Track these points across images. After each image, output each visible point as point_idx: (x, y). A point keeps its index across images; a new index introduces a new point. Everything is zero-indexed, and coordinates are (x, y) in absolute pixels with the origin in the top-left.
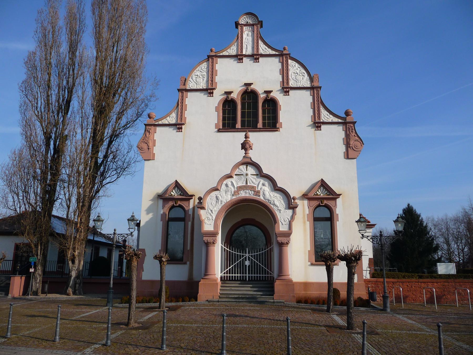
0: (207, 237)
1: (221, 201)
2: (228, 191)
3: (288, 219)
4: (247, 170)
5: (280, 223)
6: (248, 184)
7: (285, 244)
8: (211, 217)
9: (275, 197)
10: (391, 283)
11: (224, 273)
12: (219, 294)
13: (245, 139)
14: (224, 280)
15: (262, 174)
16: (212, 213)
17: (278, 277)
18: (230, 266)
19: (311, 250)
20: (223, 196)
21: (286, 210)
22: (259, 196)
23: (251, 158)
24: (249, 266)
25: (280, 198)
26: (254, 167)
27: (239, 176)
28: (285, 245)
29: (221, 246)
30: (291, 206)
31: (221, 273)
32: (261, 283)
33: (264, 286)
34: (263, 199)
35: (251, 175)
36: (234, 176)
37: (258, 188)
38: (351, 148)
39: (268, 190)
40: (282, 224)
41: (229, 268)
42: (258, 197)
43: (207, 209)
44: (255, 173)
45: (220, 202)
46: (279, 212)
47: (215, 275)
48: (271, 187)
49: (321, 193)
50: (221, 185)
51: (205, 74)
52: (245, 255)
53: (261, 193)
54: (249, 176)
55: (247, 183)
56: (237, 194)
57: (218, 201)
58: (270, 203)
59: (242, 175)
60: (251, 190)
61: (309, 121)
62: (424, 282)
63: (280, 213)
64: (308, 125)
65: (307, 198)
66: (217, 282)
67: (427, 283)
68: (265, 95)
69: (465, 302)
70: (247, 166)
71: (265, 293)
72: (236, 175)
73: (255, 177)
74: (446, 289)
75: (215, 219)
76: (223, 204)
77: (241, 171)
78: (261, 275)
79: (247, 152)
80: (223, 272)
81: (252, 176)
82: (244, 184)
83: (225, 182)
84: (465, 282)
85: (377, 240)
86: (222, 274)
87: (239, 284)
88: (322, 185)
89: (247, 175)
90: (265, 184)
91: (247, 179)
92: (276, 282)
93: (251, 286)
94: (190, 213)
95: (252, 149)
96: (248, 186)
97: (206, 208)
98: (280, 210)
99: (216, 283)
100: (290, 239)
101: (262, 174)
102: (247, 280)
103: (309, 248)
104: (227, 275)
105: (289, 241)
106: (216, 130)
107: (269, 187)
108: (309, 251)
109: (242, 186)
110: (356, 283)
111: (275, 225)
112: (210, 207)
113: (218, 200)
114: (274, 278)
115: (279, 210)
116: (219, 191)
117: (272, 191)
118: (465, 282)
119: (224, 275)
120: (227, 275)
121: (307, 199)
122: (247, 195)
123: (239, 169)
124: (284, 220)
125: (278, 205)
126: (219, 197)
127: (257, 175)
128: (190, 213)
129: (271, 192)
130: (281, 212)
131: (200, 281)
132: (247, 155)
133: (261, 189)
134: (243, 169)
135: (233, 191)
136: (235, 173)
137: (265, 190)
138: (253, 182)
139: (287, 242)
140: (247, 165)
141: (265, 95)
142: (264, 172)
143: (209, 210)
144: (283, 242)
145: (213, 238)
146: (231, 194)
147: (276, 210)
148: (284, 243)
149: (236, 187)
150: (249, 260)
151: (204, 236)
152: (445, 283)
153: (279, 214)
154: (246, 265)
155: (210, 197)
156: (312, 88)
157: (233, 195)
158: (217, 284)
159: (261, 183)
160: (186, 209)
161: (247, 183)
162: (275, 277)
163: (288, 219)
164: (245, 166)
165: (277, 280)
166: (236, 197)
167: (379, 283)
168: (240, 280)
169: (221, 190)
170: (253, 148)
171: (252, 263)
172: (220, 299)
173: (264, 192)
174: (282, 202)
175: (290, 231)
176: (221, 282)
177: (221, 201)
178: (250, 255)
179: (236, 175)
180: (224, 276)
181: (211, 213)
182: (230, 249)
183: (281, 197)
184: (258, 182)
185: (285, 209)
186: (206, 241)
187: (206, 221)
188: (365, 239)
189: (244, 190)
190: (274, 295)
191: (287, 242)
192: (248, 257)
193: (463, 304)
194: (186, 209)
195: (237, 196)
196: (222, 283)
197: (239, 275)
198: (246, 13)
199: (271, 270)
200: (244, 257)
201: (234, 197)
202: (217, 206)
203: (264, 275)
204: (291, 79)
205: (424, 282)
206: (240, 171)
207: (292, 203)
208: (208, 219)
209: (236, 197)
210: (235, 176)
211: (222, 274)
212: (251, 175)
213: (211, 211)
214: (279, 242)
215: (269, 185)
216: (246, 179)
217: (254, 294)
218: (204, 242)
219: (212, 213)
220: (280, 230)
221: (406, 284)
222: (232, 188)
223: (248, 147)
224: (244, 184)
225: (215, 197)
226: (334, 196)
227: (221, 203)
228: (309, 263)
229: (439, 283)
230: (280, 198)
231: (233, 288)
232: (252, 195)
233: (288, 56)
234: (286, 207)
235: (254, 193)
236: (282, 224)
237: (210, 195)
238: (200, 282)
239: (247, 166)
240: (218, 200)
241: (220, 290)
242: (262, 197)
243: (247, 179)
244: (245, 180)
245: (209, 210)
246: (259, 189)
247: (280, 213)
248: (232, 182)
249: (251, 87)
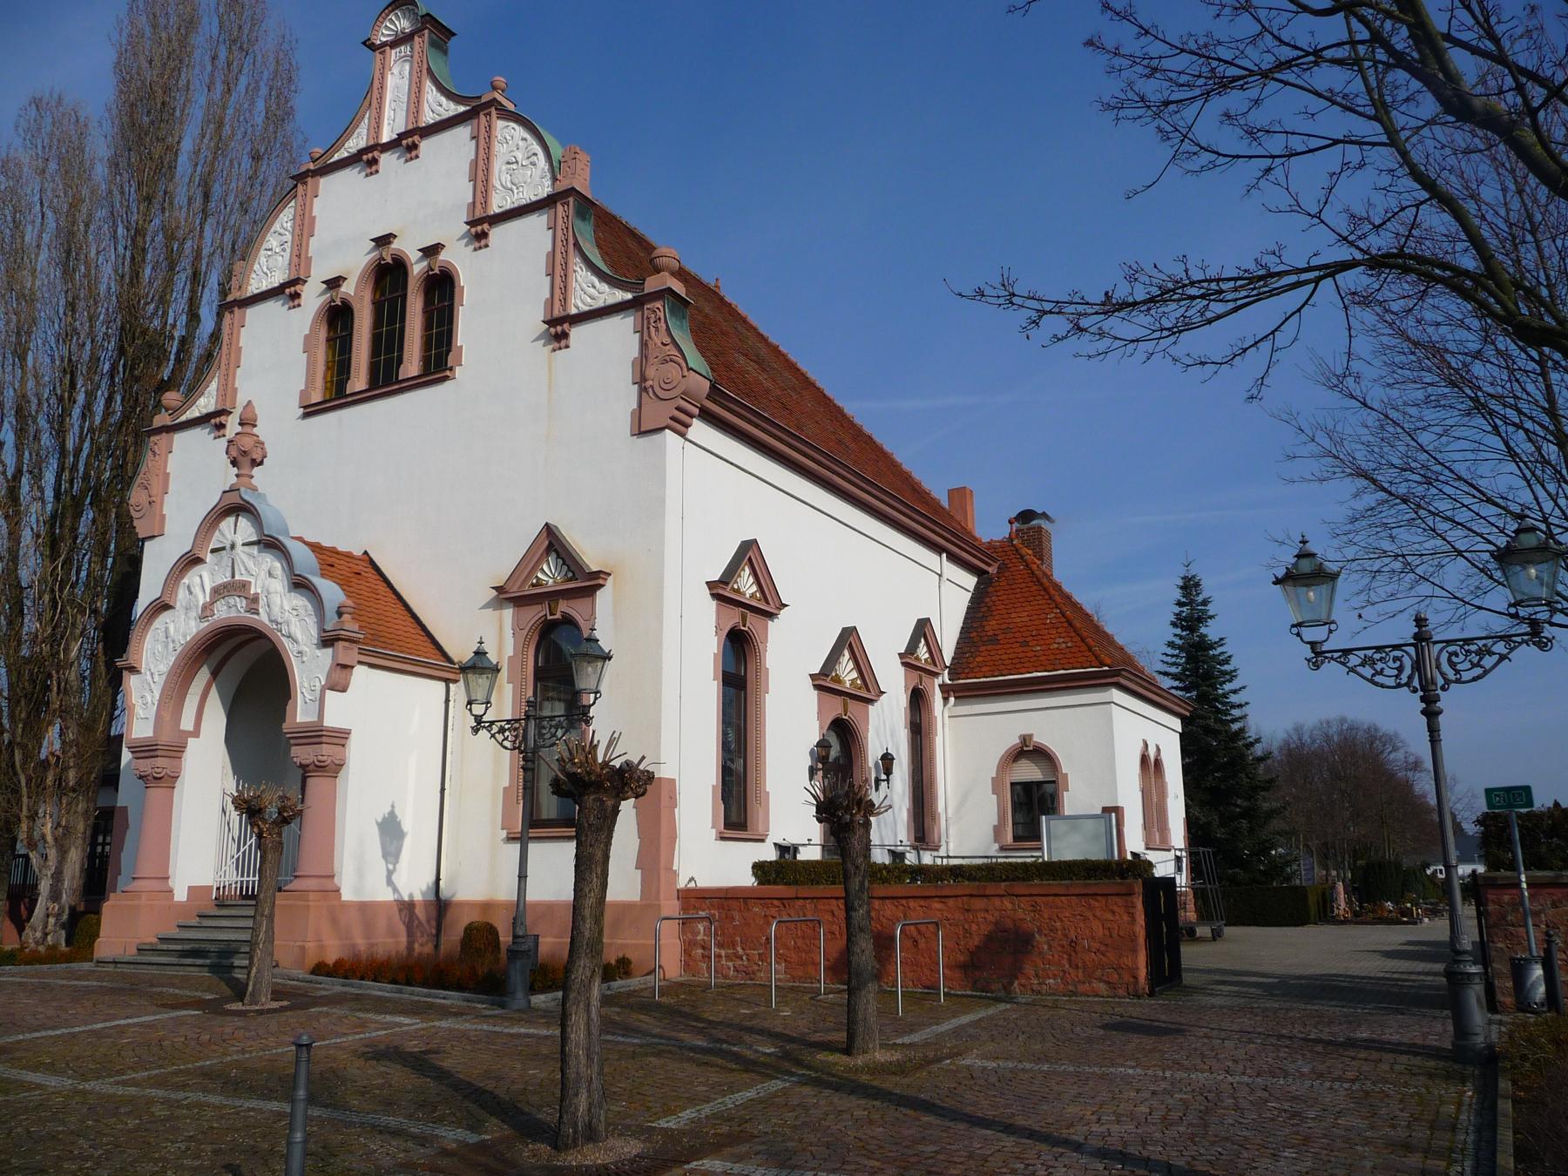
10: (776, 902)
18: (244, 845)
19: (510, 786)
23: (224, 492)
34: (267, 622)
35: (243, 545)
36: (209, 558)
38: (651, 394)
49: (549, 574)
51: (288, 237)
54: (239, 548)
61: (534, 318)
62: (893, 898)
64: (534, 337)
67: (904, 902)
68: (425, 263)
69: (1051, 981)
72: (213, 551)
73: (254, 550)
74: (974, 927)
81: (246, 549)
84: (1055, 895)
85: (516, 737)
88: (551, 548)
91: (233, 559)
103: (506, 782)
108: (505, 788)
110: (626, 907)
118: (1055, 895)
125: (300, 640)
129: (288, 595)
141: (425, 263)
152: (973, 900)
156: (1417, 206)
167: (734, 904)
169: (178, 606)
172: (139, 955)
179: (213, 551)
188: (483, 733)
193: (1039, 992)
198: (390, 5)
204: (500, 188)
205: (893, 898)
210: (209, 554)
221: (827, 907)
225: (163, 629)
226: (586, 583)
228: (504, 834)
229: (951, 902)
232: (242, 610)
233: (493, 109)
237: (152, 628)
242: (263, 617)
243: (233, 559)
249: (393, 246)
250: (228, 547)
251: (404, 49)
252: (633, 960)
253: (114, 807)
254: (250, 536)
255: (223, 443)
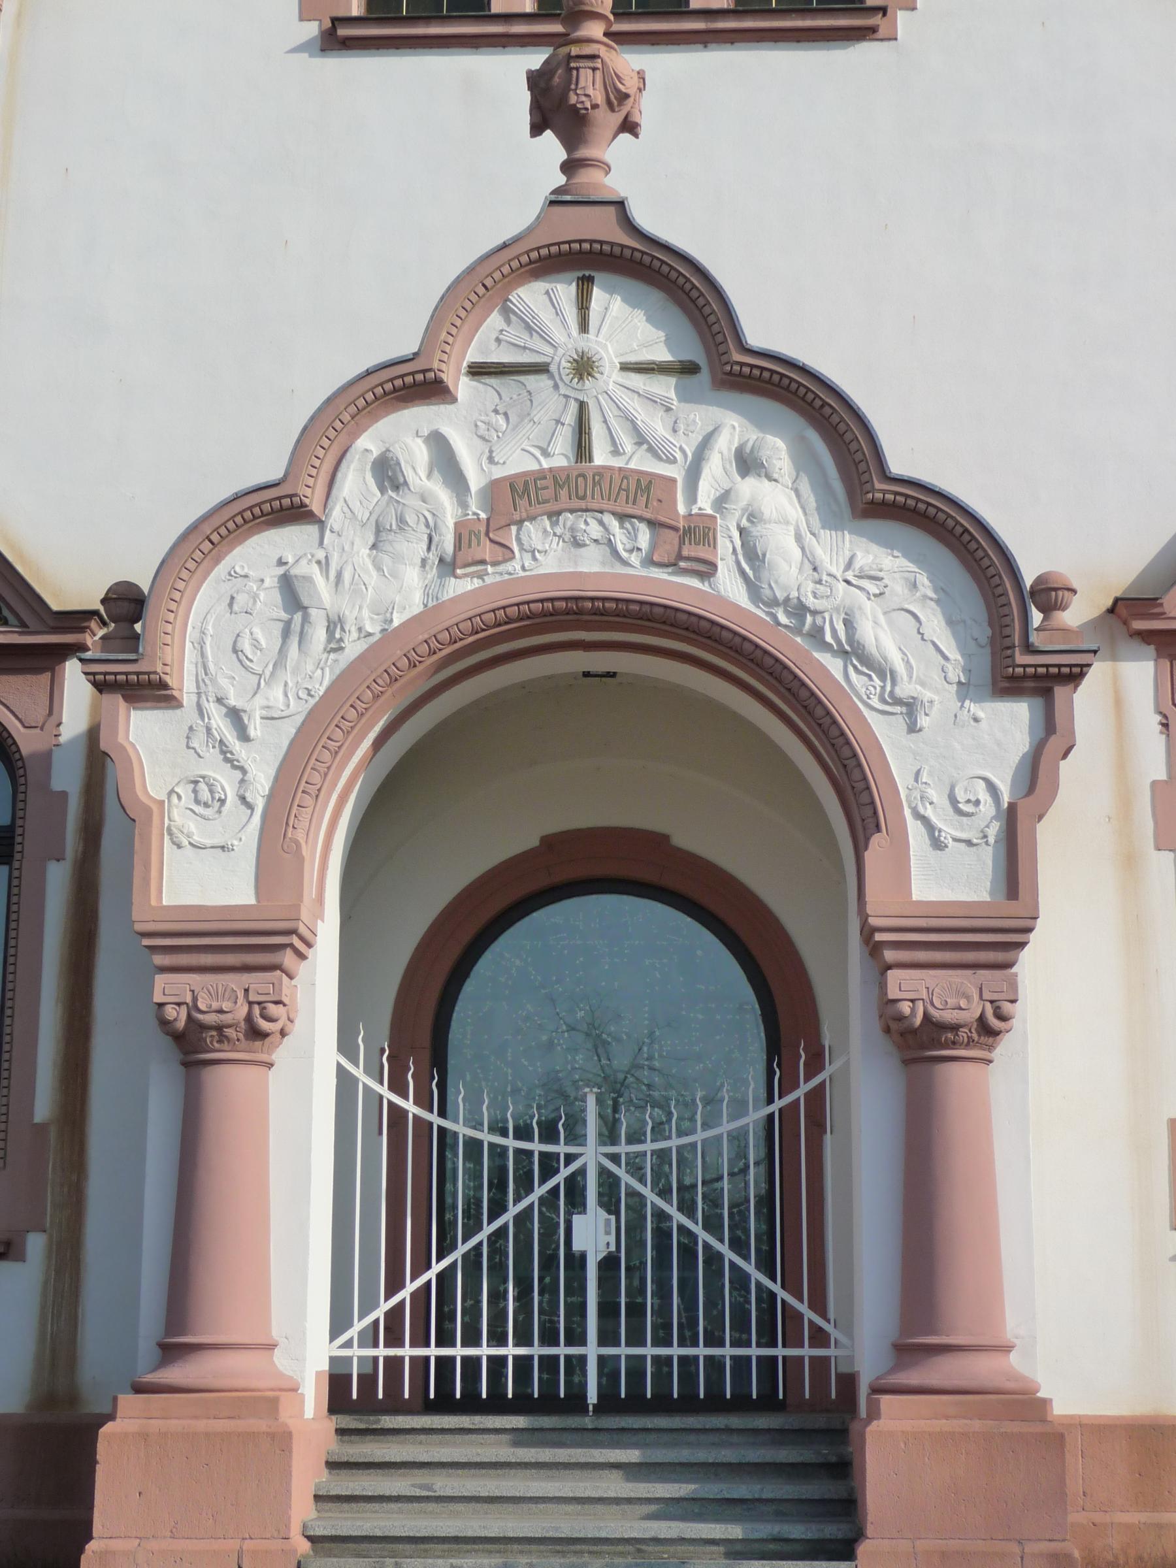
0: (194, 979)
1: (334, 624)
2: (401, 520)
3: (992, 788)
4: (584, 326)
5: (915, 832)
6: (601, 457)
7: (963, 1034)
8: (227, 782)
9: (865, 583)
11: (370, 1337)
12: (304, 1546)
13: (562, 180)
14: (367, 1405)
15: (737, 357)
16: (244, 737)
17: (898, 1367)
20: (347, 576)
21: (974, 708)
22: (707, 569)
23: (620, 204)
24: (609, 1264)
25: (914, 586)
26: (656, 296)
27: (508, 386)
28: (970, 1044)
29: (340, 1069)
30: (1021, 658)
31: (338, 1324)
32: (729, 1430)
33: (754, 1455)
35: (626, 367)
36: (464, 387)
37: (692, 497)
39: (794, 512)
40: (937, 844)
41: (411, 1287)
42: (694, 582)
43: (188, 698)
44: (663, 355)
45: (319, 635)
46: (900, 723)
47: (271, 1347)
48: (821, 486)
50: (327, 467)
52: (570, 1159)
53: (726, 548)
54: (610, 377)
55: (582, 449)
56: (487, 550)
57: (306, 619)
58: (816, 635)
59: (540, 369)
60: (622, 517)
63: (913, 728)
65: (1147, 637)
66: (286, 1415)
70: (585, 284)
71: (764, 1530)
72: (478, 371)
73: (665, 387)
75: (271, 798)
76: (353, 648)
77: (523, 338)
78: (675, 1351)
79: (583, 153)
80: (359, 1326)
81: (637, 381)
82: (560, 457)
83: (369, 443)
86: (348, 1344)
87: (520, 1437)
89: (584, 367)
90: (764, 455)
91: (582, 406)
92: (874, 1413)
93: (632, 1455)
94: (57, 784)
95: (629, 127)
96: (602, 471)
97: (186, 686)
98: (911, 707)
99: (272, 1436)
100: (1013, 985)
101: (737, 357)
102: (592, 1397)
104: (522, 1351)
105: (1007, 1007)
106: (312, 30)
107: (805, 487)
109: (541, 475)
111: (859, 848)
112: (223, 682)
113: (298, 617)
114: (848, 1382)
115: (898, 702)
116: (312, 530)
117: (831, 522)
119: (370, 1352)
120: (522, 1351)
121: (1151, 649)
122: (591, 562)
123: (507, 312)
124: (953, 801)
126: (308, 579)
127: (687, 369)
128: (57, 784)
129: (825, 534)
130: (923, 721)
131: (111, 1417)
132: (587, 176)
133: (722, 500)
134: (546, 316)
135: (451, 525)
136: (473, 355)
137: (768, 510)
138: (641, 440)
139: (982, 1020)
140: (590, 280)
142: (754, 339)
143: (212, 708)
144: (949, 1016)
145: (246, 979)
146: (433, 558)
147: (875, 702)
148: (955, 1028)
149: (475, 481)
150: (609, 1201)
151: (159, 960)
153: (909, 741)
154: (583, 1256)
155: (227, 588)
157: (448, 567)
158: (282, 1441)
159: (725, 445)
160: (25, 749)
161: (582, 449)
162: (867, 1373)
163: (992, 788)
164: (565, 290)
165: (885, 1399)
166: (477, 583)
168: (522, 1404)
169: (336, 517)
170: (646, 121)
171: (635, 1243)
173: (755, 531)
174: (935, 625)
175: (1013, 908)
176: (330, 1424)
177: (334, 624)
178: (615, 1158)
179: (478, 371)
180: (394, 1365)
181: (231, 738)
182: (423, 1100)
183: (923, 580)
184: (696, 438)
185: (965, 690)
186: (178, 1017)
187: (181, 816)
189: (554, 515)
190: (862, 1549)
191: (982, 1020)
192: (605, 1175)
194: (27, 742)
195: (493, 575)
196: (341, 1432)
197: (511, 1351)
199: (819, 1304)
200: (565, 1172)
201: (460, 586)
202: (296, 671)
203: (754, 1351)
206: (515, 334)
207: (1034, 638)
208: (205, 795)
209: (477, 583)
211: (348, 1344)
212: (626, 367)
213: (235, 716)
214: (900, 1018)
215: (803, 460)
216: (573, 407)
217: (656, 1541)
218: (165, 1024)
219: (244, 737)
220: (914, 898)
222: (444, 497)
223: (599, 97)
224: (560, 457)
225: (271, 581)
227: (335, 646)
230: (914, 586)
231: (444, 1484)
232: (634, 559)
234: (967, 671)
235: (654, 546)
236: (937, 844)
237: (221, 570)
238: (107, 1429)
239: (585, 284)
240: (298, 617)
241: (318, 1498)
243: (582, 406)
244: (570, 418)
245: (212, 708)
246: (704, 503)
247: (913, 728)
248: (439, 445)
250: (562, 364)
251: (981, 557)
252: (454, 521)
253: (1156, 660)
254: (646, 345)
255: (871, 592)
